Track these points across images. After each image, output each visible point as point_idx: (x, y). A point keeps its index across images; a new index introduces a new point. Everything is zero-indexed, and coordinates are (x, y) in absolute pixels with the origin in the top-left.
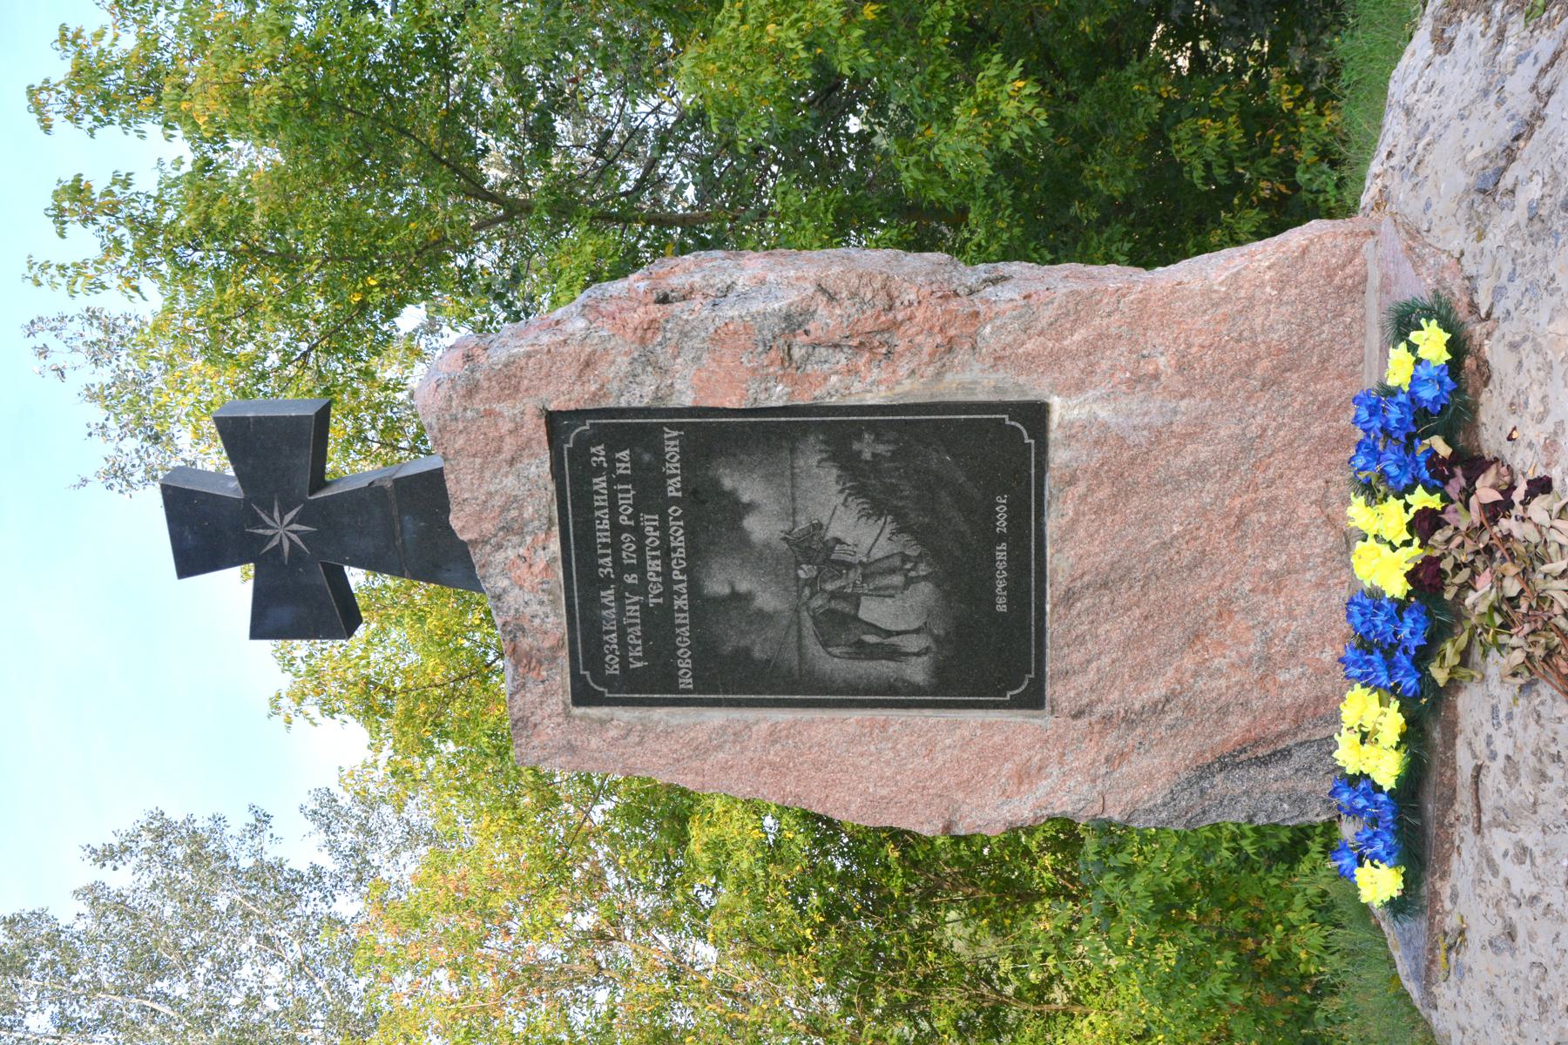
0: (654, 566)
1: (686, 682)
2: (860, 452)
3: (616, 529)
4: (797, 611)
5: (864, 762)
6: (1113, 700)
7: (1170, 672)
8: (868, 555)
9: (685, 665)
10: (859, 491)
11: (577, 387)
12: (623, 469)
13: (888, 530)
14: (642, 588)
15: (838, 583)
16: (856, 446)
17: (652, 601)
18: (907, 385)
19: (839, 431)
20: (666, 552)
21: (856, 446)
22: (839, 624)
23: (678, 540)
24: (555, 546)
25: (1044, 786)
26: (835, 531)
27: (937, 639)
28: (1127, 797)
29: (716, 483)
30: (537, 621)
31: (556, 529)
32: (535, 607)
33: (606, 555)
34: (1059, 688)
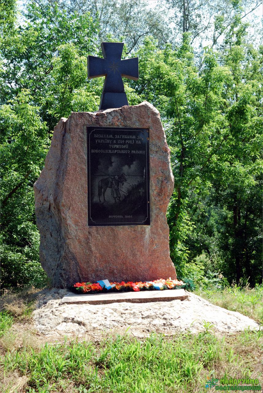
0: (117, 146)
1: (93, 151)
2: (140, 189)
3: (125, 139)
4: (108, 175)
5: (77, 188)
6: (92, 240)
7: (96, 251)
8: (120, 190)
9: (97, 151)
10: (133, 189)
11: (154, 135)
12: (137, 142)
13: (125, 194)
14: (112, 144)
15: (114, 184)
16: (142, 188)
17: (110, 145)
19: (145, 184)
20: (121, 149)
21: (142, 188)
22: (106, 184)
23: (123, 152)
24: (121, 127)
25: (74, 226)
26: (125, 184)
27: (103, 204)
28: (71, 243)
29: (134, 161)
30: (105, 121)
31: (124, 127)
32: (109, 121)
33: (120, 137)
34: (95, 228)
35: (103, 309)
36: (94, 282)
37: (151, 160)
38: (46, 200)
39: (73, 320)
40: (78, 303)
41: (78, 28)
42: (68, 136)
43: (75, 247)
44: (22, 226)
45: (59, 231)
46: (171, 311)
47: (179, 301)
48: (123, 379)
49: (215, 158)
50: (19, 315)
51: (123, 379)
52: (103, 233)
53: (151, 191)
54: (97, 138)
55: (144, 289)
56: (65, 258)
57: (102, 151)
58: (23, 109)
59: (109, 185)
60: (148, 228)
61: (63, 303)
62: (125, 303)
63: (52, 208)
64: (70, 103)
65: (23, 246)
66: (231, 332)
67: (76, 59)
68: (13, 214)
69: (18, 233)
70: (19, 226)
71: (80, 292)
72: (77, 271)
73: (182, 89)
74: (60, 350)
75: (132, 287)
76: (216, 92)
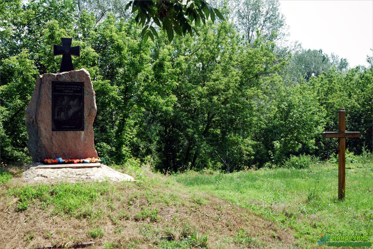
1: (55, 93)
12: (78, 89)
18: (86, 117)
19: (82, 110)
20: (69, 93)
22: (61, 110)
23: (70, 94)
24: (69, 81)
26: (71, 110)
35: (57, 171)
36: (54, 159)
37: (85, 99)
38: (31, 118)
39: (42, 176)
40: (45, 168)
41: (63, 7)
42: (42, 85)
43: (45, 141)
44: (23, 134)
45: (37, 133)
46: (91, 172)
47: (96, 168)
48: (62, 199)
49: (146, 93)
50: (15, 174)
51: (62, 199)
52: (60, 134)
53: (84, 114)
54: (57, 87)
55: (80, 163)
56: (40, 147)
57: (59, 94)
58: (23, 61)
59: (63, 110)
60: (83, 133)
61: (38, 168)
62: (69, 168)
63: (34, 122)
64: (54, 58)
65: (24, 147)
66: (119, 181)
67: (58, 30)
68: (18, 128)
69: (20, 139)
70: (21, 134)
71: (47, 164)
72: (46, 154)
73: (125, 52)
74: (34, 187)
75: (74, 161)
76: (146, 53)
